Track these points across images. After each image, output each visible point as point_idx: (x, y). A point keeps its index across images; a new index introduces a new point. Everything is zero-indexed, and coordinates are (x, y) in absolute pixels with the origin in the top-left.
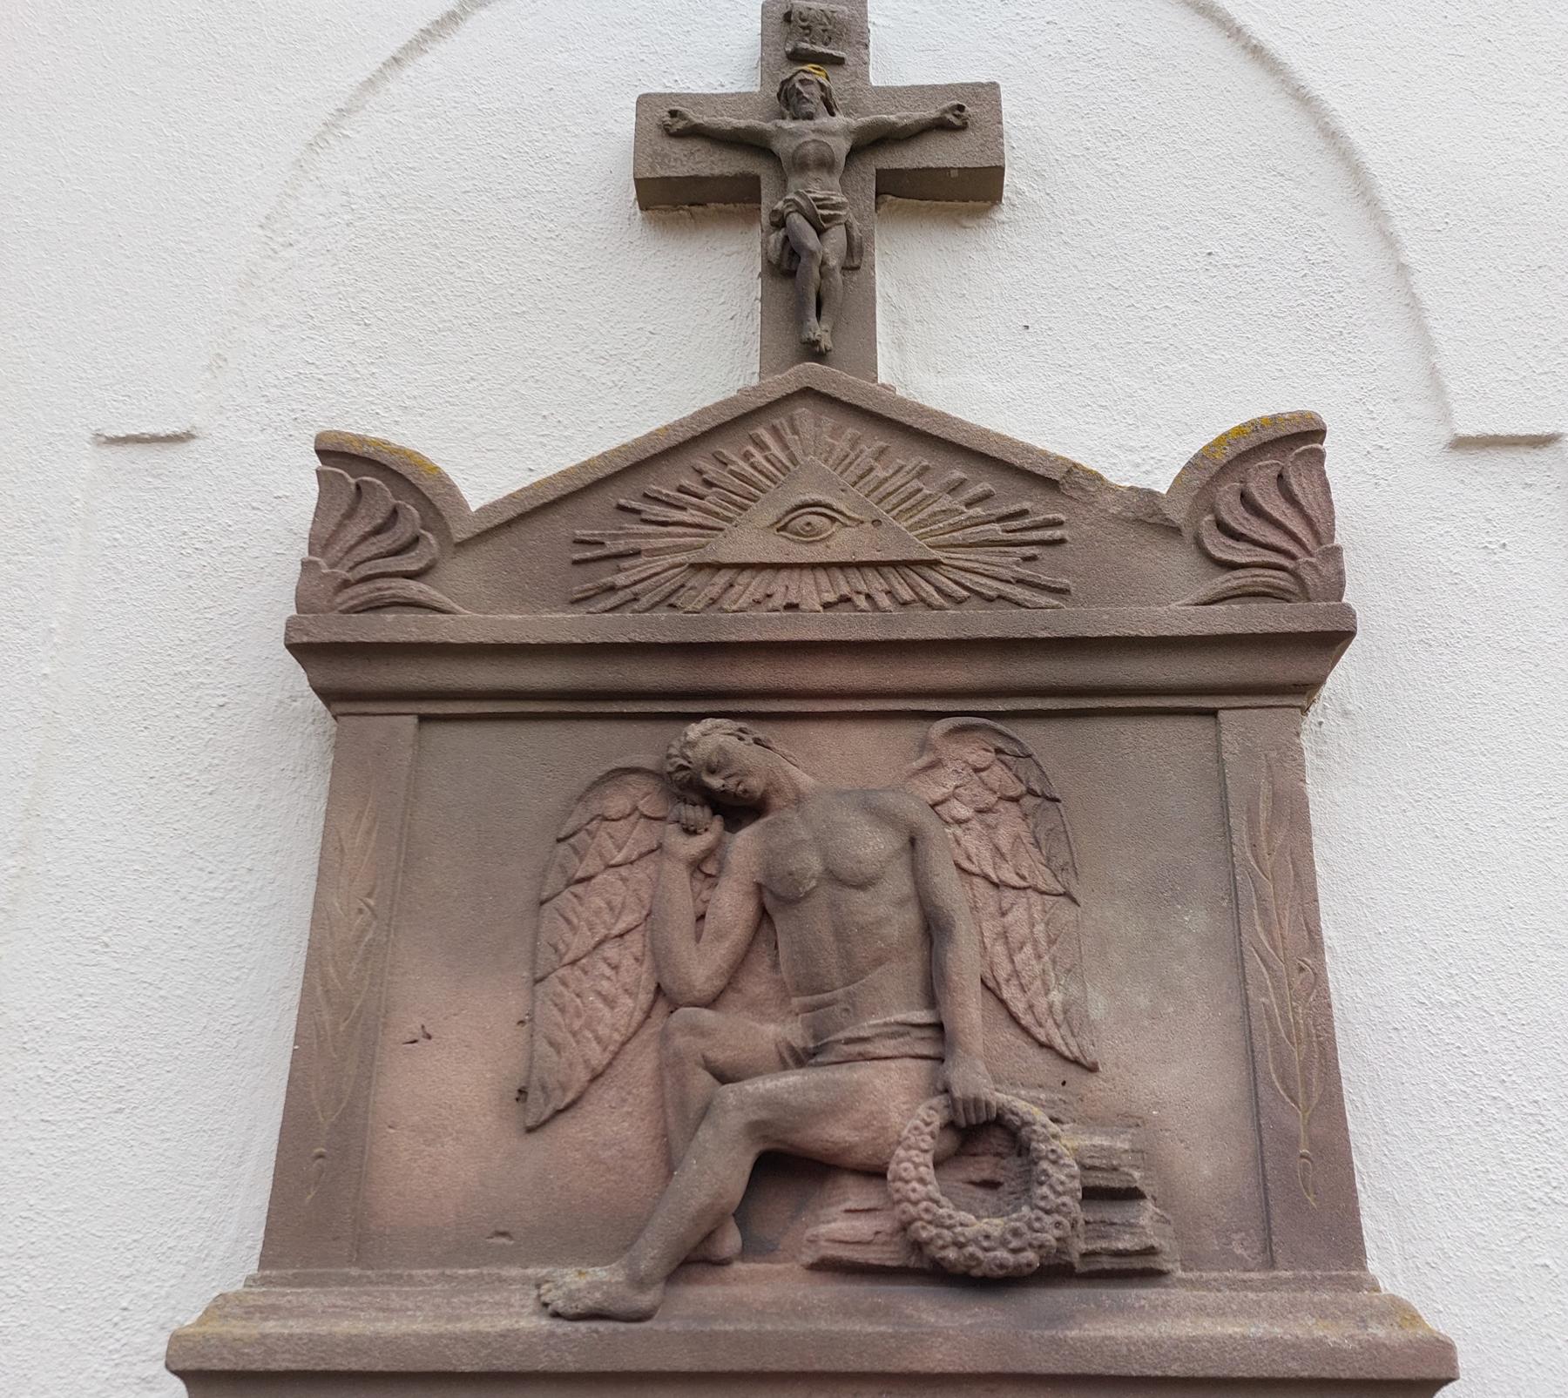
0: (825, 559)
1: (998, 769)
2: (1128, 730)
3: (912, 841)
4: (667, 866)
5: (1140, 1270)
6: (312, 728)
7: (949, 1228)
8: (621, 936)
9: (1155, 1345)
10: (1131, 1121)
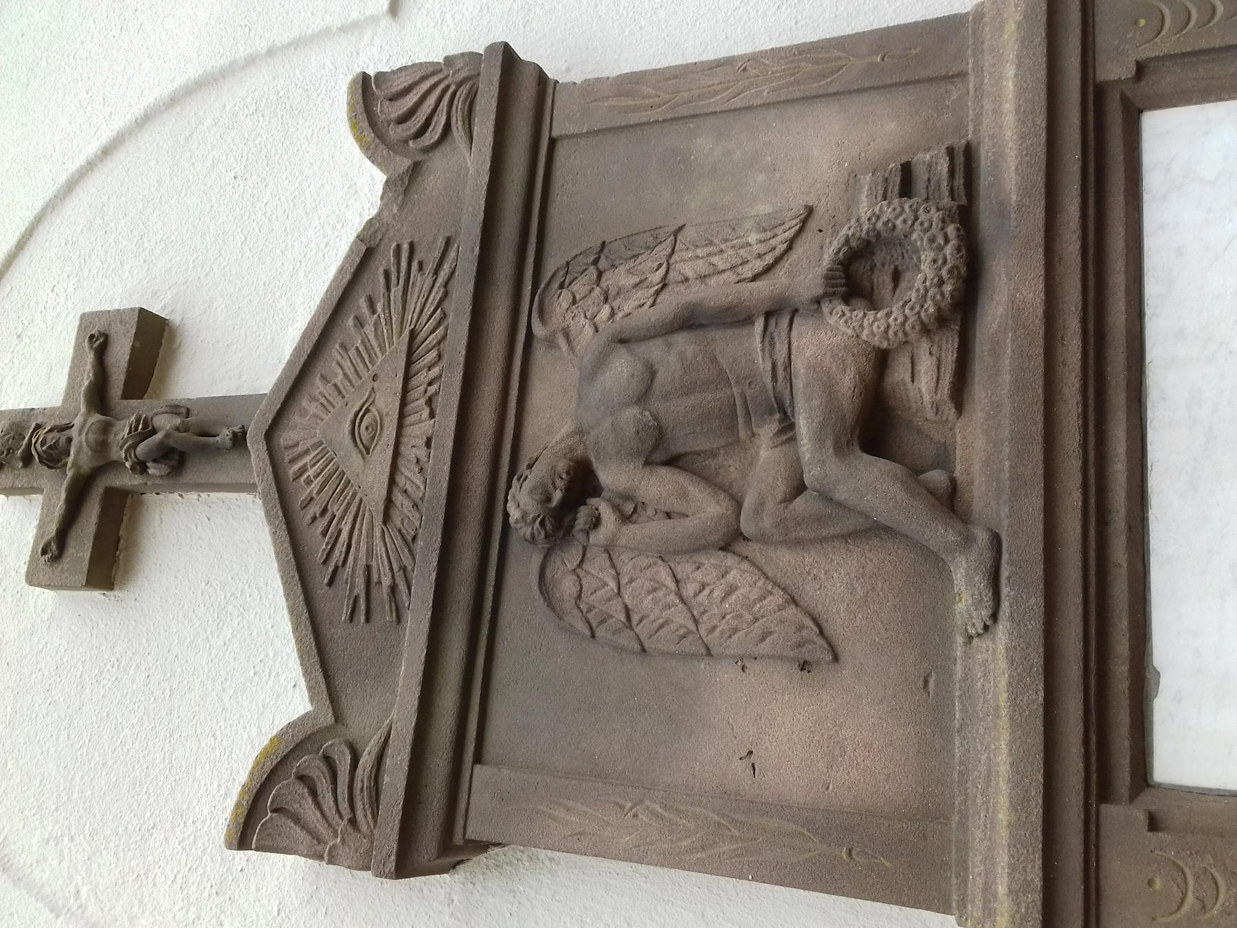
0: (396, 416)
1: (575, 287)
2: (555, 211)
3: (622, 341)
4: (623, 541)
5: (965, 162)
6: (478, 886)
7: (926, 291)
8: (677, 582)
9: (1022, 137)
10: (852, 180)
